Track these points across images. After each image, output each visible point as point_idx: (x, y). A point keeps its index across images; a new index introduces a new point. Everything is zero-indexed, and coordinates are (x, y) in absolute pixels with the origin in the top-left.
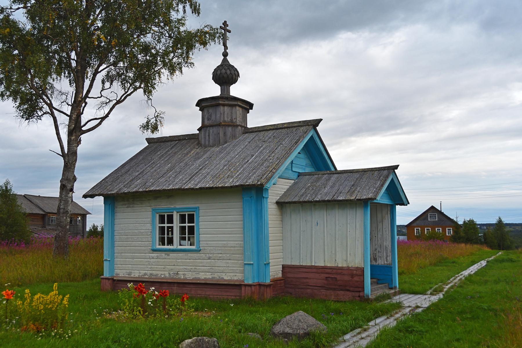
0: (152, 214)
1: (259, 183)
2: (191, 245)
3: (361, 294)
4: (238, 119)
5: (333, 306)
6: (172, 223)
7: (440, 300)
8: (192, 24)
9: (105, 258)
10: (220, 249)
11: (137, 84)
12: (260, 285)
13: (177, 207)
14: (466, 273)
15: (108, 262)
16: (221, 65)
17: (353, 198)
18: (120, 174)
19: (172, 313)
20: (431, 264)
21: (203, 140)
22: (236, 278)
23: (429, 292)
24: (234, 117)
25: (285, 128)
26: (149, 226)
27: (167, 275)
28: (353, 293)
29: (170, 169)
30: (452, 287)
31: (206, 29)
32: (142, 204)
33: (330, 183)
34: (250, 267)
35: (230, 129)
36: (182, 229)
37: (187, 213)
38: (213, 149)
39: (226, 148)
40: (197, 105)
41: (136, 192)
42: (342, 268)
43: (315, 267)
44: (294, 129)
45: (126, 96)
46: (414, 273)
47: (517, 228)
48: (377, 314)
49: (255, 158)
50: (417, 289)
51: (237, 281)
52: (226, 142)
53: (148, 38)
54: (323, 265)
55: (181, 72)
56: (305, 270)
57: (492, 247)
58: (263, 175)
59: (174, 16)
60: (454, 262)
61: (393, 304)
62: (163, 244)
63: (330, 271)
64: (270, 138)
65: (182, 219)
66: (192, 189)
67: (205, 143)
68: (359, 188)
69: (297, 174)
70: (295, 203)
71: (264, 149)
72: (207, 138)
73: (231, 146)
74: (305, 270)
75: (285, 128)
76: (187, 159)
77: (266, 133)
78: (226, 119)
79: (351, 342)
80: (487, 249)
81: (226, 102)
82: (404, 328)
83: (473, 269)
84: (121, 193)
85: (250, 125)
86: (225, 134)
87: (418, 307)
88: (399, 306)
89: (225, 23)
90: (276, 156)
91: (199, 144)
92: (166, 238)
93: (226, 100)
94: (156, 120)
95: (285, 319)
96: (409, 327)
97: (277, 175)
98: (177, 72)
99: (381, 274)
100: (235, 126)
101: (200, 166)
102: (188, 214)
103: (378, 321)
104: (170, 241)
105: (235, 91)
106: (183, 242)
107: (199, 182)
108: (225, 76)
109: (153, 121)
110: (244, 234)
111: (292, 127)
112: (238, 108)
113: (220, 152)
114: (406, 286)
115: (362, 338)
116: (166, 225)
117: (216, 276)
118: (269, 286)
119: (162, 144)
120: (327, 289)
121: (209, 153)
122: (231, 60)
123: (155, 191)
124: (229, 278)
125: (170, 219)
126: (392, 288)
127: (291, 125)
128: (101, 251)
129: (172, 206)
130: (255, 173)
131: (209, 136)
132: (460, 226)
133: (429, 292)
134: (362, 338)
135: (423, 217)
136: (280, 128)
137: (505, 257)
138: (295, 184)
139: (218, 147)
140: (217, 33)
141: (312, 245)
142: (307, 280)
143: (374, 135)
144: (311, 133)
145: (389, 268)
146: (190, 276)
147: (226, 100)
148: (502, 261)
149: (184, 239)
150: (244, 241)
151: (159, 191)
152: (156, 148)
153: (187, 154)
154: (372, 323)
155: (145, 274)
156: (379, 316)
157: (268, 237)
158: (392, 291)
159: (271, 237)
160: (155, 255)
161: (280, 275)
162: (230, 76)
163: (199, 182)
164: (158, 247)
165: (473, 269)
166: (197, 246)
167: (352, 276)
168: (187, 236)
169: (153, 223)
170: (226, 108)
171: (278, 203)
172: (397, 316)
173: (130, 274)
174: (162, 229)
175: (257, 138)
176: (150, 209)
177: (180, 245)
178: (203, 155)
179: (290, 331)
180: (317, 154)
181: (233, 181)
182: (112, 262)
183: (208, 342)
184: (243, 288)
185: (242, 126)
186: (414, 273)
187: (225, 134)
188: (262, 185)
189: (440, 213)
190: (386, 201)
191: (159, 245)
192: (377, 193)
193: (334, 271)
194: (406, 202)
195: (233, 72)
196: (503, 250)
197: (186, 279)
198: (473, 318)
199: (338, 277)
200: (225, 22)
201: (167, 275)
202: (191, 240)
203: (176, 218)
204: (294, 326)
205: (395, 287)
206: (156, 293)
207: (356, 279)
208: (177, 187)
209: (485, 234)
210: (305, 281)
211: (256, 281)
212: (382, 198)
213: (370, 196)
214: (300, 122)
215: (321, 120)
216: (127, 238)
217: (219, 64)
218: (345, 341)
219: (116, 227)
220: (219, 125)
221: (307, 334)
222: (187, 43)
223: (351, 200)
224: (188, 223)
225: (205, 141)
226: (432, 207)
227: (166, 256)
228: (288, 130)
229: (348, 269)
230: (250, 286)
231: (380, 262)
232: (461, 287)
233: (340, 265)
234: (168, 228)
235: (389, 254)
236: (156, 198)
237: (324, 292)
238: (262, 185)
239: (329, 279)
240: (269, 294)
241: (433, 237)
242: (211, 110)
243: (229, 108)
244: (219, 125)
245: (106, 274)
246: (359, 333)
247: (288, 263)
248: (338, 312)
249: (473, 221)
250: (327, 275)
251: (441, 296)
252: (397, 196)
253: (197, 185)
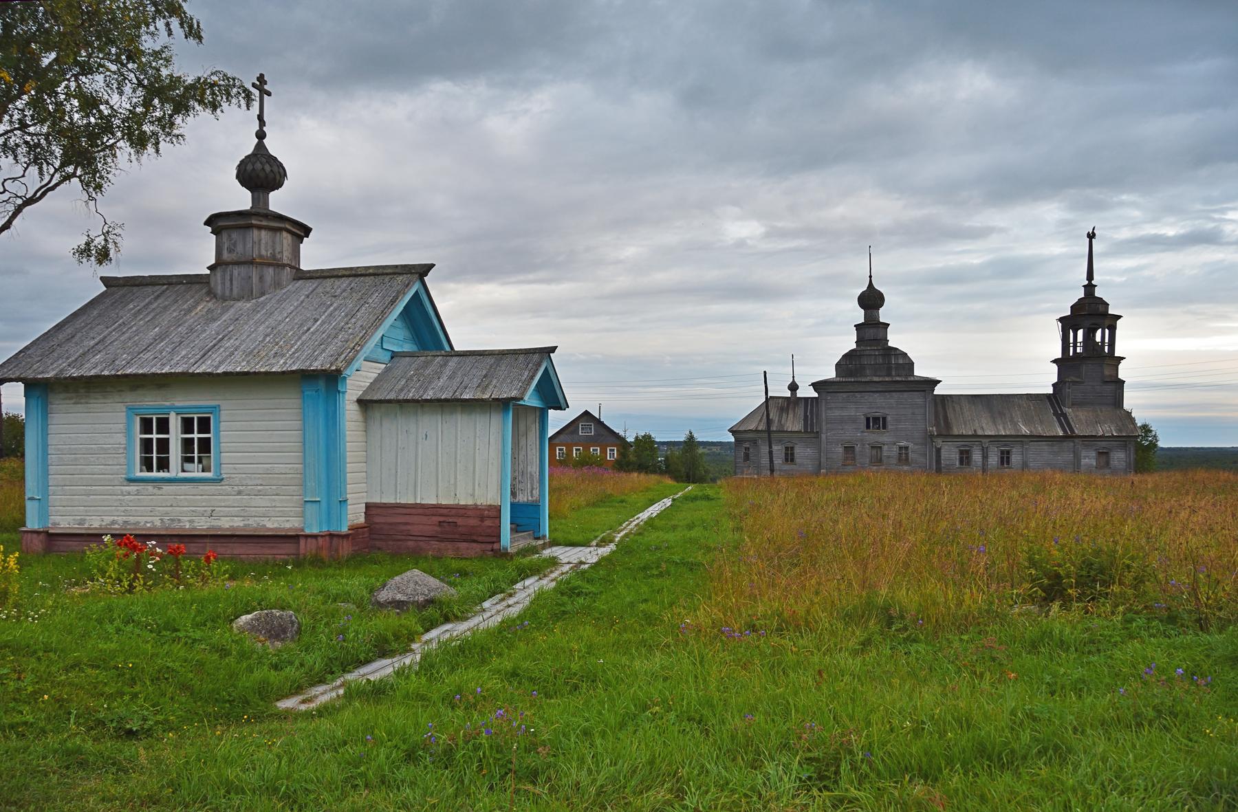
0: (128, 417)
1: (334, 368)
2: (203, 471)
3: (496, 546)
4: (285, 254)
5: (455, 564)
6: (167, 433)
7: (613, 552)
8: (187, 65)
9: (28, 495)
10: (257, 475)
11: (70, 169)
12: (331, 536)
13: (176, 406)
14: (644, 516)
15: (36, 503)
16: (254, 155)
17: (486, 396)
18: (56, 342)
19: (191, 581)
20: (588, 505)
22: (288, 526)
23: (594, 543)
24: (278, 249)
25: (370, 275)
26: (121, 438)
27: (158, 523)
28: (483, 546)
29: (161, 337)
30: (626, 535)
31: (215, 78)
32: (105, 398)
33: (447, 372)
34: (315, 506)
35: (271, 270)
36: (187, 444)
37: (195, 416)
38: (239, 304)
39: (264, 304)
41: (97, 377)
42: (465, 507)
43: (422, 506)
44: (387, 278)
45: (46, 190)
46: (566, 518)
47: (714, 449)
48: (523, 574)
49: (321, 325)
50: (579, 538)
51: (290, 529)
52: (263, 294)
53: (96, 83)
54: (434, 502)
55: (157, 151)
56: (405, 511)
57: (677, 478)
58: (339, 355)
59: (148, 44)
60: (622, 501)
61: (545, 560)
62: (150, 469)
63: (445, 511)
64: (344, 291)
65: (187, 425)
66: (209, 374)
67: (224, 294)
68: (494, 381)
69: (389, 354)
70: (389, 401)
71: (335, 309)
72: (228, 284)
73: (273, 301)
74: (405, 511)
75: (370, 275)
76: (190, 320)
77: (337, 282)
78: (263, 252)
79: (494, 611)
80: (669, 482)
81: (264, 223)
82: (568, 590)
83: (654, 510)
84: (65, 378)
85: (305, 266)
86: (261, 278)
87: (582, 563)
88: (554, 562)
89: (261, 78)
90: (359, 323)
91: (211, 294)
92: (154, 456)
93: (257, 218)
94: (106, 240)
95: (393, 582)
96: (575, 588)
97: (362, 355)
98: (150, 149)
99: (525, 517)
100: (280, 266)
101: (218, 334)
102: (199, 419)
103: (528, 582)
104: (164, 465)
105: (278, 201)
106: (187, 466)
107: (221, 363)
108: (262, 175)
109: (100, 241)
110: (304, 452)
111: (383, 274)
112: (285, 234)
113: (255, 310)
114: (559, 535)
115: (509, 606)
116: (155, 436)
117: (252, 522)
118: (346, 536)
119: (135, 289)
120: (442, 540)
121: (232, 311)
122: (273, 146)
123: (136, 375)
124: (276, 525)
125: (163, 426)
126: (538, 538)
127: (380, 271)
129: (168, 404)
130: (324, 351)
131: (231, 280)
132: (630, 444)
133: (594, 543)
134: (509, 606)
135: (571, 429)
136: (362, 275)
137: (700, 494)
138: (387, 370)
139: (248, 300)
140: (234, 86)
141: (416, 470)
142: (409, 527)
143: (488, 280)
144: (416, 287)
145: (535, 507)
146: (203, 525)
147: (257, 218)
148: (695, 499)
149: (191, 460)
150: (304, 463)
151: (143, 375)
152: (124, 296)
153: (189, 310)
154: (519, 586)
155: (113, 522)
156: (528, 577)
157: (345, 458)
158: (541, 542)
159: (350, 456)
160: (133, 488)
161: (362, 520)
162: (271, 175)
163: (221, 363)
164: (139, 474)
165: (654, 510)
166: (216, 472)
167: (482, 519)
168: (196, 455)
169: (128, 432)
170: (263, 233)
171: (361, 402)
172: (553, 576)
173: (82, 522)
174: (146, 445)
175: (320, 290)
176: (122, 407)
177: (183, 471)
178: (221, 314)
179: (404, 598)
180: (423, 324)
181: (285, 363)
182: (43, 502)
183: (281, 617)
184: (302, 542)
185: (292, 267)
186: (566, 518)
187: (261, 278)
188: (339, 371)
189: (599, 422)
190: (536, 403)
191: (141, 471)
192: (526, 390)
193: (454, 511)
194: (563, 405)
195: (275, 169)
196: (694, 482)
197: (195, 529)
198: (661, 575)
199: (460, 521)
200: (262, 76)
201: (158, 523)
202: (204, 461)
203: (175, 424)
204: (409, 591)
205: (544, 537)
206: (158, 550)
207: (488, 523)
208: (179, 370)
209: (667, 458)
210: (404, 528)
211: (325, 529)
212: (531, 399)
213: (514, 394)
214: (396, 266)
215: (433, 265)
216: (76, 459)
217: (250, 152)
218: (484, 610)
219: (52, 440)
220: (251, 262)
221: (430, 602)
222: (179, 97)
223: (482, 400)
224: (158, 433)
225: (223, 288)
226: (586, 413)
227: (156, 491)
228: (378, 280)
229: (476, 507)
230: (315, 537)
231: (522, 498)
232: (640, 534)
233: (462, 503)
235: (536, 485)
236: (134, 388)
237: (435, 544)
238: (339, 371)
240: (346, 549)
241: (585, 462)
243: (270, 233)
244: (251, 262)
245: (32, 523)
246: (503, 600)
247: (376, 499)
248: (464, 574)
249: (650, 437)
250: (442, 519)
251: (612, 547)
252: (552, 396)
253: (217, 367)
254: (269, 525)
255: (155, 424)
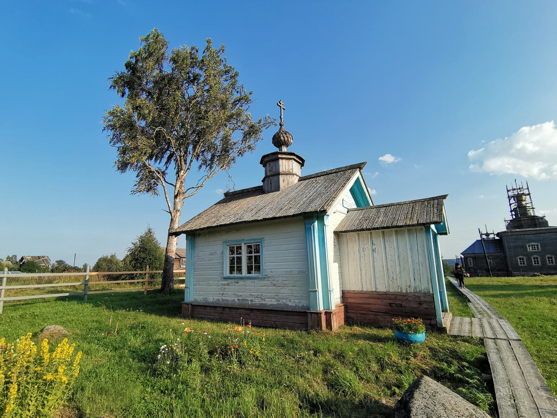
13: (245, 238)
21: (266, 187)
24: (291, 167)
40: (261, 163)
72: (270, 186)
92: (235, 265)
103: (390, 331)
104: (240, 270)
116: (235, 256)
128: (197, 232)
167: (420, 303)
174: (232, 261)
184: (313, 314)
199: (404, 304)
234: (238, 258)
236: (238, 230)
239: (394, 305)
242: (272, 164)
254: (290, 304)
255: (235, 250)
